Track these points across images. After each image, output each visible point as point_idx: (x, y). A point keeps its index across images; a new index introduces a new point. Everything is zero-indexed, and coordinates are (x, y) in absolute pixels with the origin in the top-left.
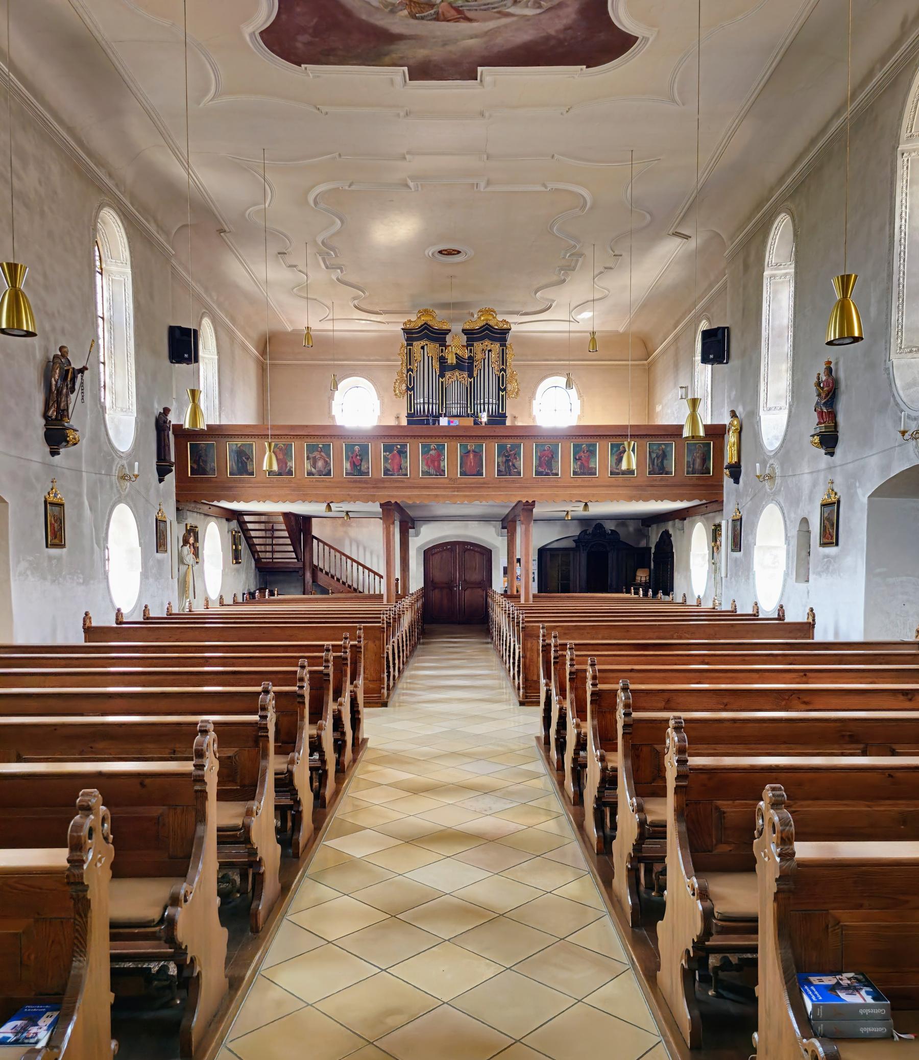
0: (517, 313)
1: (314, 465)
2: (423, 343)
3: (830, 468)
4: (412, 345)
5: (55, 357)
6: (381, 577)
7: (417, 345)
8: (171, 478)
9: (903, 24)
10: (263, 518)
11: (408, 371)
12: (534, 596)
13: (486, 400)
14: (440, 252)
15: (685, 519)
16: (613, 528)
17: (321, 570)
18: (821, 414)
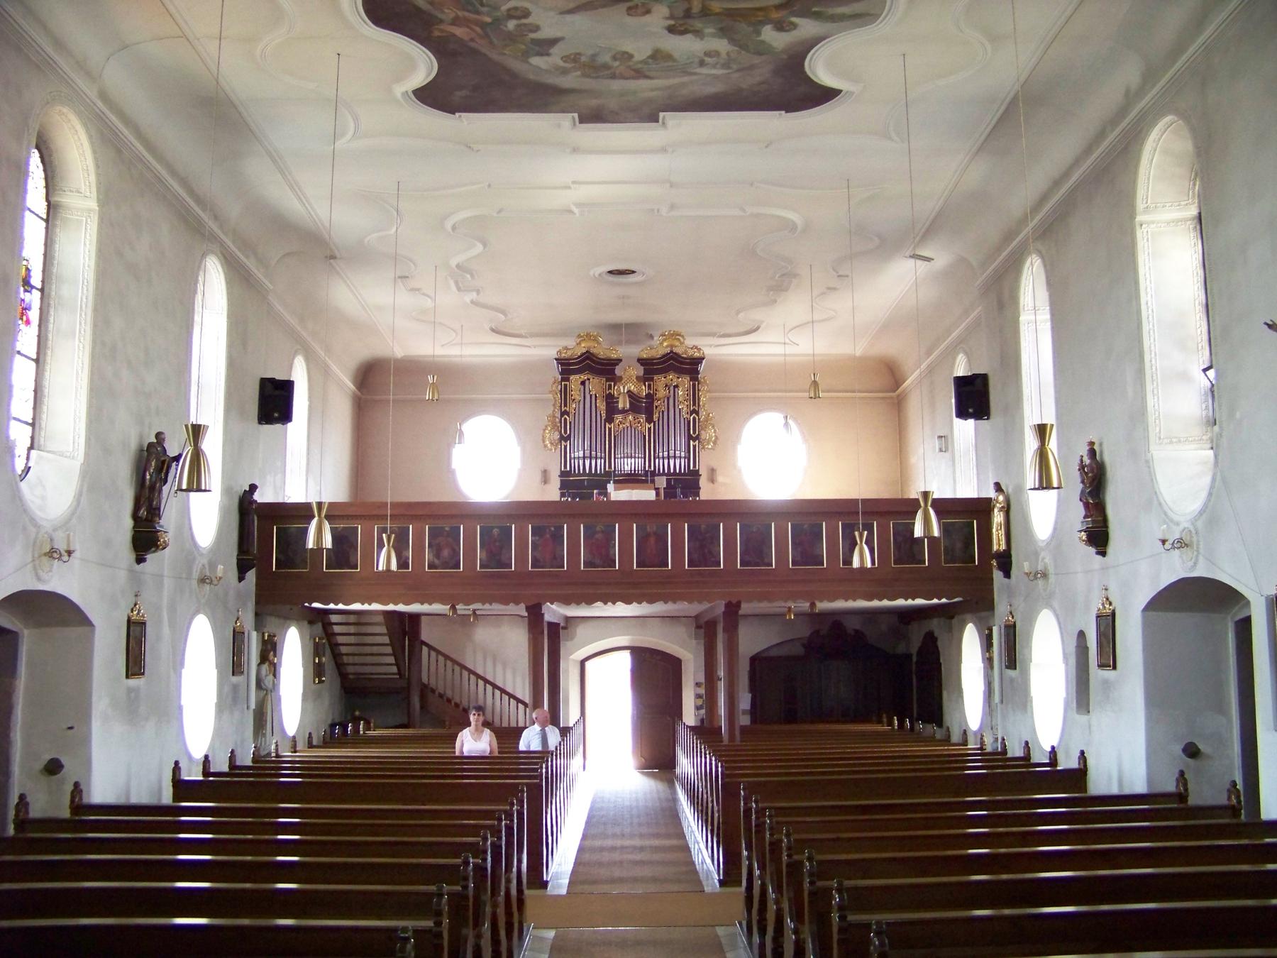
0: (713, 335)
1: (438, 555)
2: (584, 377)
3: (1104, 569)
4: (568, 380)
5: (150, 445)
6: (526, 705)
7: (575, 379)
8: (251, 575)
9: (1127, 92)
10: (352, 619)
11: (562, 414)
12: (744, 730)
13: (672, 453)
14: (610, 272)
15: (952, 617)
16: (858, 627)
17: (433, 691)
18: (1087, 505)
